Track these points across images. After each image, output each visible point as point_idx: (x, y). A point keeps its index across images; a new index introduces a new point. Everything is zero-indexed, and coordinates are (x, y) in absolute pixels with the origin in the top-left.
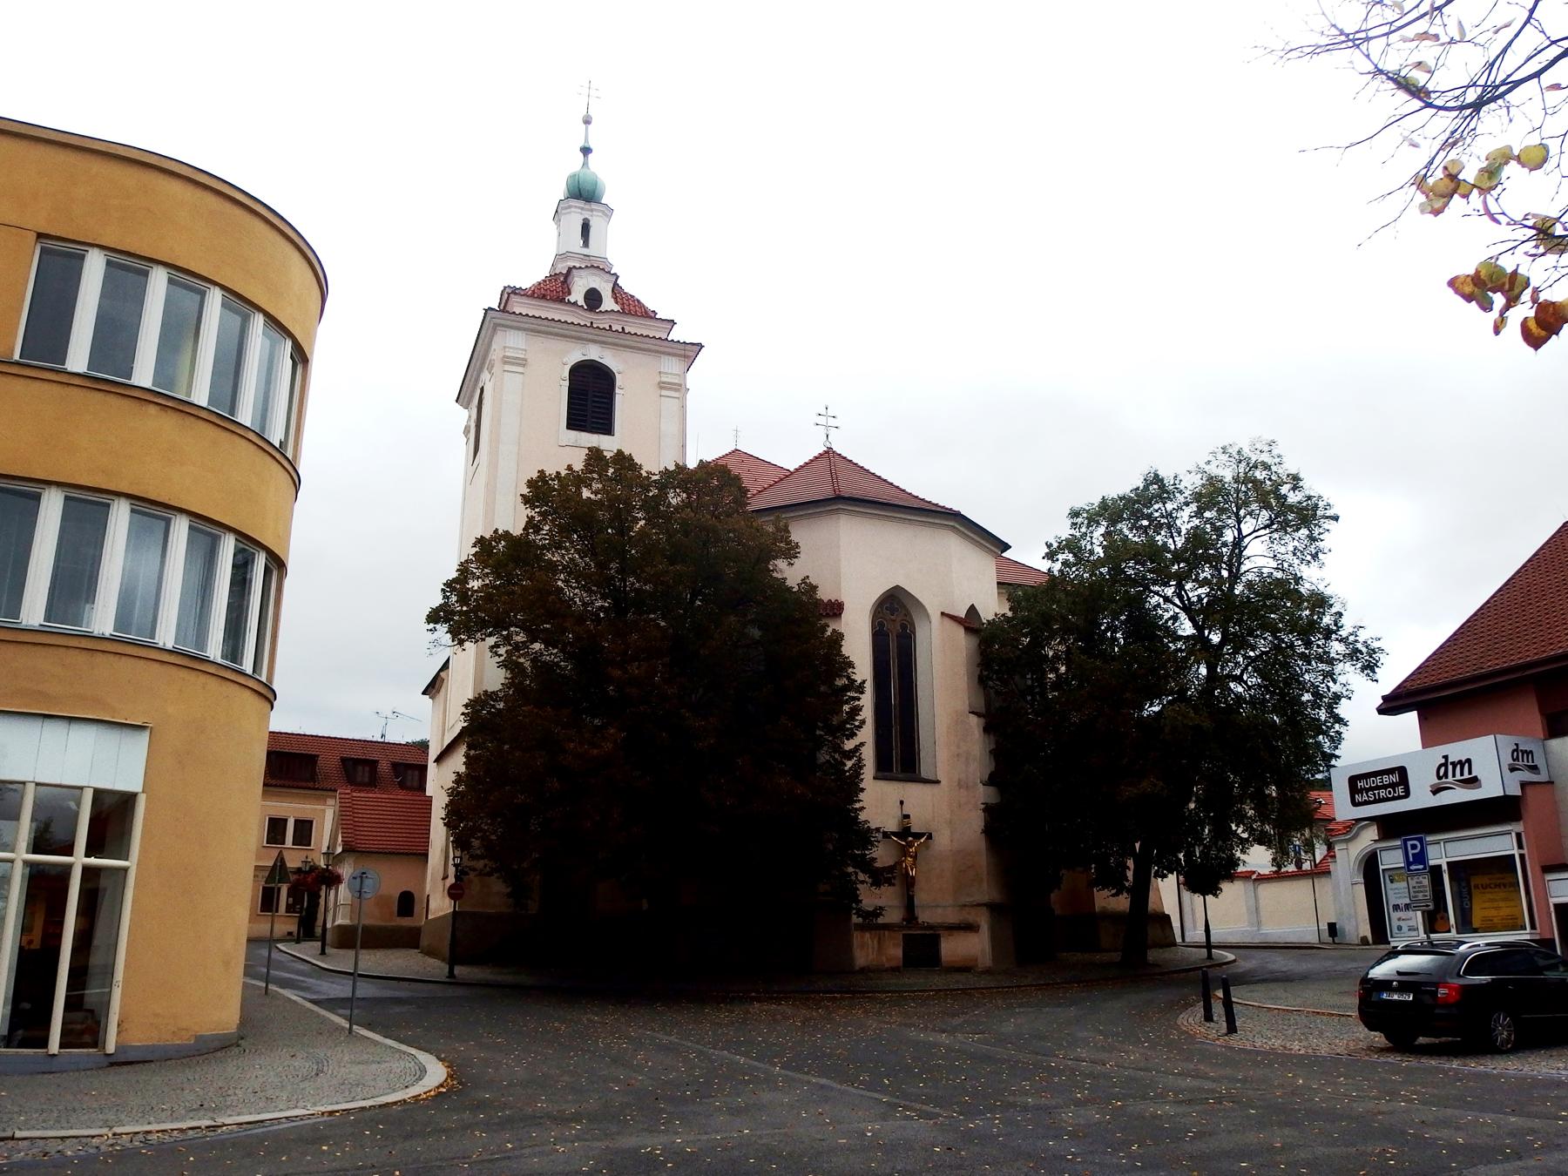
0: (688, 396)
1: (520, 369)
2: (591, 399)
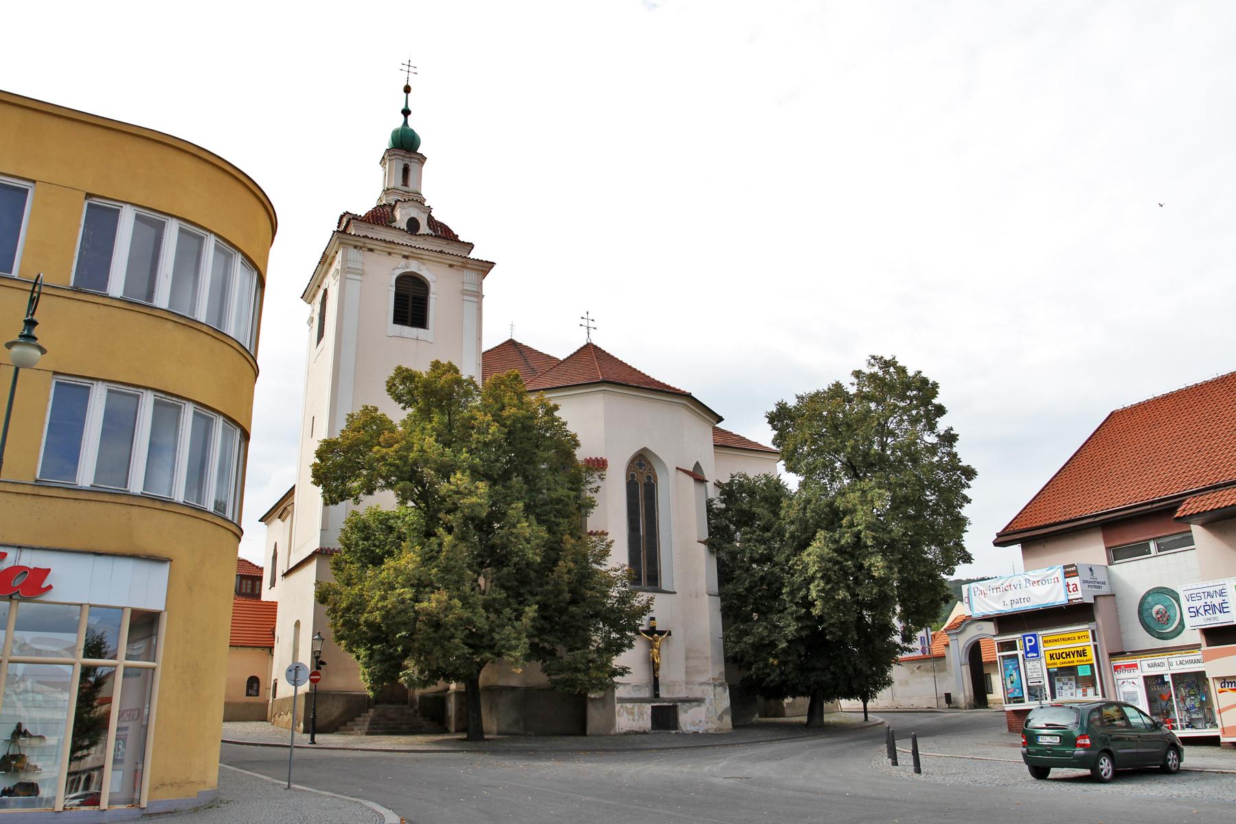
1: (359, 277)
2: (411, 305)
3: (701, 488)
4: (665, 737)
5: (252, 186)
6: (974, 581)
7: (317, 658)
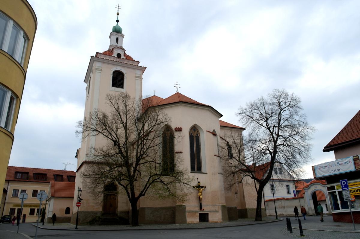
0: (143, 80)
1: (100, 72)
2: (118, 80)
3: (215, 138)
4: (204, 224)
5: (30, 7)
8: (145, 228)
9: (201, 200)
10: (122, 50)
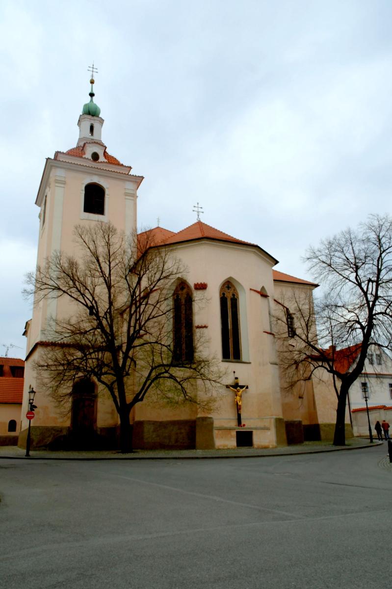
1: (63, 186)
2: (94, 199)
6: (367, 487)
7: (31, 404)
8: (145, 456)
9: (240, 409)
10: (101, 147)
